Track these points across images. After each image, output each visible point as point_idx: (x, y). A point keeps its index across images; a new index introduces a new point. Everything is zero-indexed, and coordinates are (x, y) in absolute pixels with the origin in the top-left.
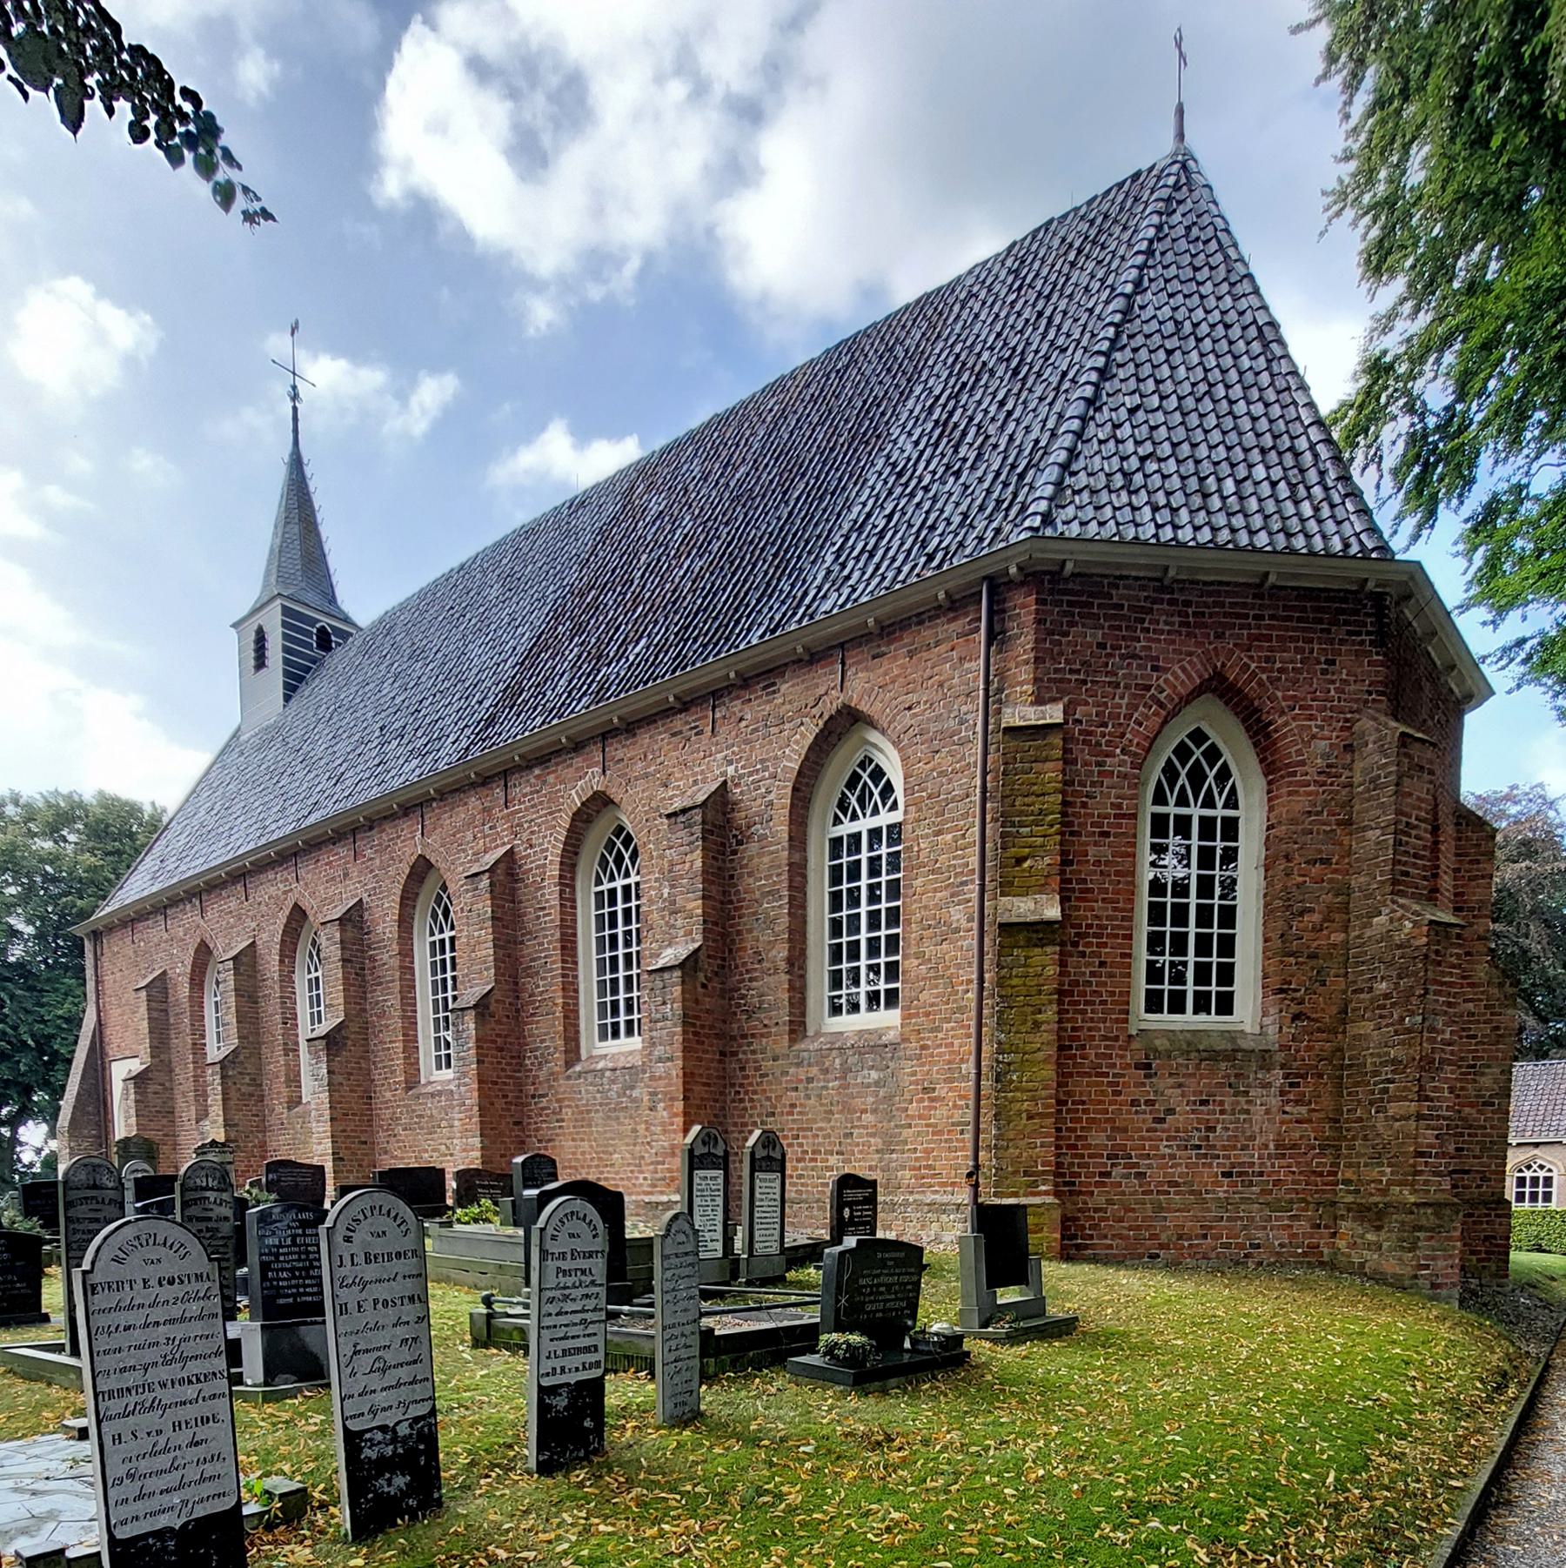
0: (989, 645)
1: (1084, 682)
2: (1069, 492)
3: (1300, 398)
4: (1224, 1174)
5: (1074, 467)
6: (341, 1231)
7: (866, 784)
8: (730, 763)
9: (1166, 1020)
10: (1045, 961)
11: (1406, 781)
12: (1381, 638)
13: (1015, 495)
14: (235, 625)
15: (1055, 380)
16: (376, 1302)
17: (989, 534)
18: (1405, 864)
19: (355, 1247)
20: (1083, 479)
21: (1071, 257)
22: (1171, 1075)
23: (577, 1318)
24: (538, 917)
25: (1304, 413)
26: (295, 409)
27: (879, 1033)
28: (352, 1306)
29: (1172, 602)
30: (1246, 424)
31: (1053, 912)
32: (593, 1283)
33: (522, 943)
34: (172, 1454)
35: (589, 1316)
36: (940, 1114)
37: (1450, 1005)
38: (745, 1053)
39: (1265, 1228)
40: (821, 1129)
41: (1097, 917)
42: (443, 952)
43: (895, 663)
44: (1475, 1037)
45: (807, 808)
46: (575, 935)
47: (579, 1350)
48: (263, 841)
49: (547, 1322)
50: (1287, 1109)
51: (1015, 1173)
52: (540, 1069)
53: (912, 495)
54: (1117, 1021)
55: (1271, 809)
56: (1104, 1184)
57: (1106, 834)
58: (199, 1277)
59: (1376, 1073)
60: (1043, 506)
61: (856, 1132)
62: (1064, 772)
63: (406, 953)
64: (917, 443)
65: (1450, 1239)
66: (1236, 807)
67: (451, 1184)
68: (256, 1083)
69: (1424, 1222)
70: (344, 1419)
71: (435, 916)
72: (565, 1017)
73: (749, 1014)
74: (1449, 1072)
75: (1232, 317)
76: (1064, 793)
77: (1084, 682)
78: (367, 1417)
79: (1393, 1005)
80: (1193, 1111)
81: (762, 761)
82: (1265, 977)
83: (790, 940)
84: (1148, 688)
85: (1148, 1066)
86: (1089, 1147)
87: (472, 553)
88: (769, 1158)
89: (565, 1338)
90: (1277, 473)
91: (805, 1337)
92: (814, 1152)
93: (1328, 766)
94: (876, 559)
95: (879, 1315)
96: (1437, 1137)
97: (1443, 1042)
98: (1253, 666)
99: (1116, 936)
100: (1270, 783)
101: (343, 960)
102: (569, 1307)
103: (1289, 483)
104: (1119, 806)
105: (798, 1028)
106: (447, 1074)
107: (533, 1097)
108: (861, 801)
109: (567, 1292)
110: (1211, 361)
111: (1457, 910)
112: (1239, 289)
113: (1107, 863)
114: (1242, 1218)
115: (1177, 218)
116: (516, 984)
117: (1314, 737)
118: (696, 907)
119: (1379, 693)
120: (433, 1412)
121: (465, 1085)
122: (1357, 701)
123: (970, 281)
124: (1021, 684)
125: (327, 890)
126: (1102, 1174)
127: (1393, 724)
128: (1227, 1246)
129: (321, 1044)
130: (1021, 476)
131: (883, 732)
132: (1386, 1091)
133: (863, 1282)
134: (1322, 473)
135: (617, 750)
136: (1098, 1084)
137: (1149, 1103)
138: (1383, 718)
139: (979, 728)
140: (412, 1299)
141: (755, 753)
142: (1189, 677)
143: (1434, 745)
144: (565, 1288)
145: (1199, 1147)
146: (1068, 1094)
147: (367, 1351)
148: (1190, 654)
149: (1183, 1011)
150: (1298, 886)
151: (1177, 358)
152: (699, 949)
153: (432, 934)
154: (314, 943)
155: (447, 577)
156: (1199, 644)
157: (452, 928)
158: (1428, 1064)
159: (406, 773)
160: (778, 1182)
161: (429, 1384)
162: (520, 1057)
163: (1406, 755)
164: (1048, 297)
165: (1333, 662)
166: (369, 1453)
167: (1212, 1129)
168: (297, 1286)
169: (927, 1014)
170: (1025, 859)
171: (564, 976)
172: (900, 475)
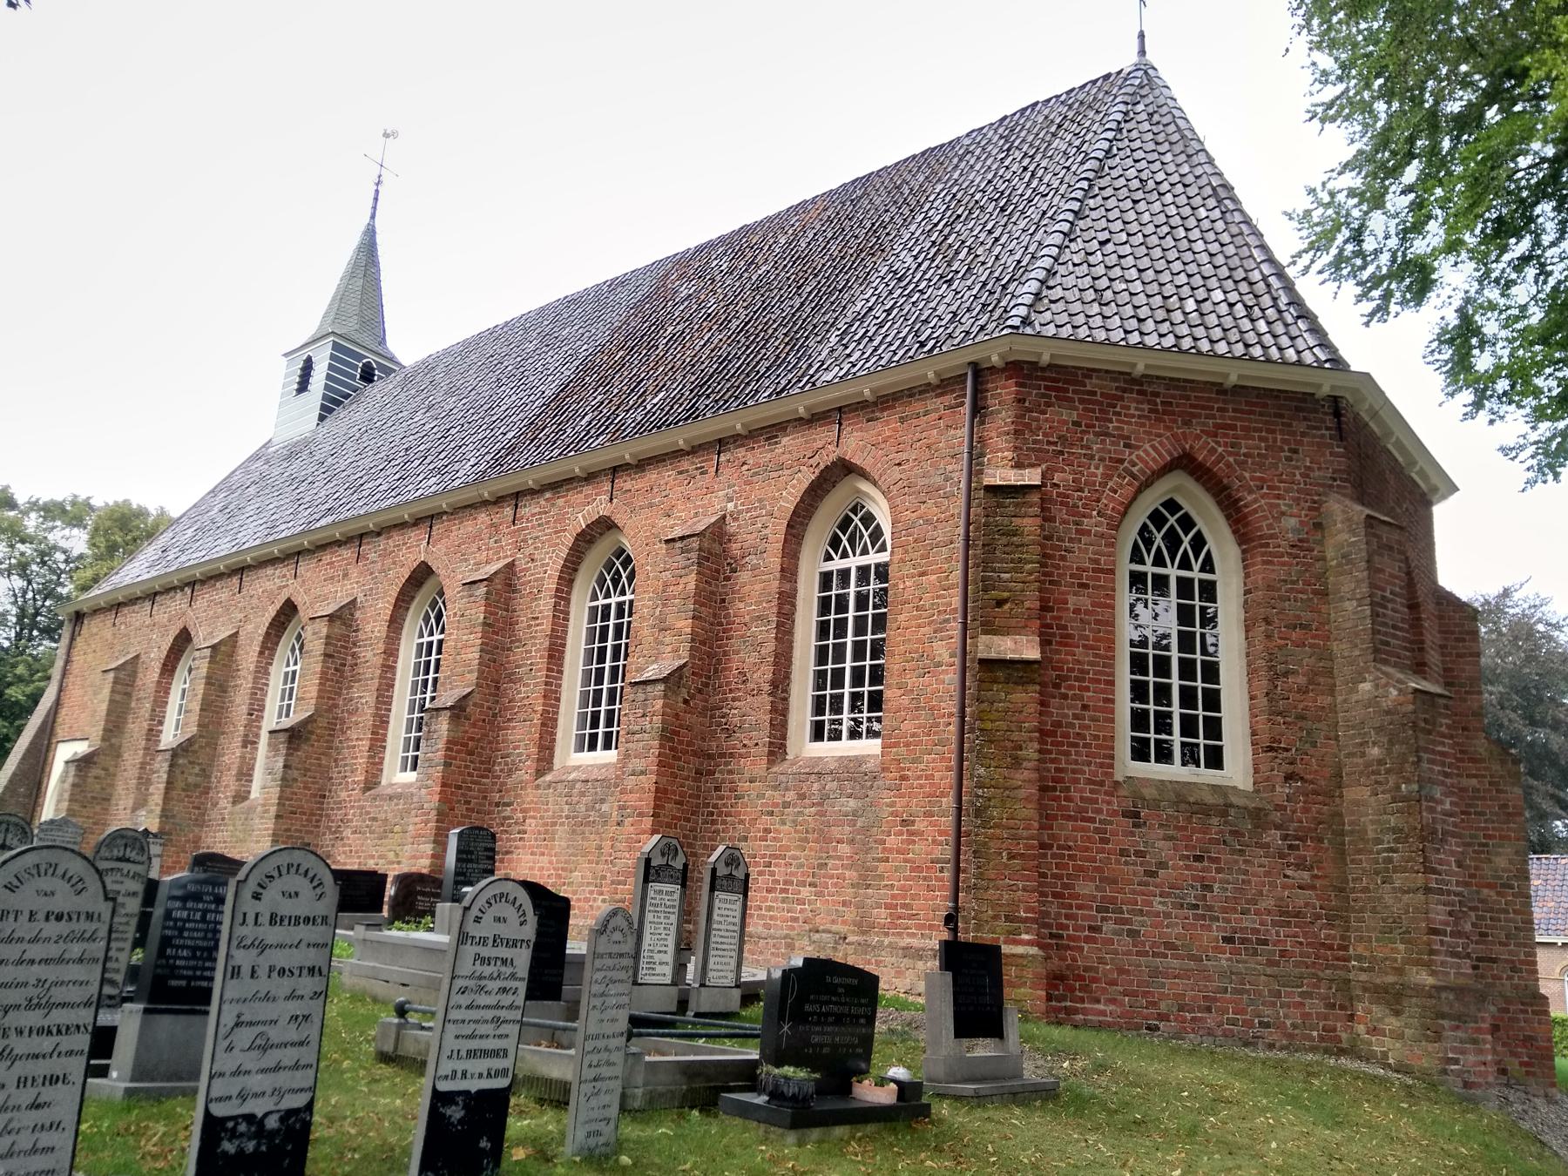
0: (973, 416)
1: (1062, 453)
2: (1046, 301)
3: (1252, 240)
4: (1225, 939)
5: (1051, 283)
6: (252, 886)
7: (853, 528)
8: (730, 500)
9: (1153, 770)
10: (1024, 698)
11: (1376, 558)
12: (1341, 433)
13: (999, 301)
14: (286, 355)
15: (1036, 217)
16: (271, 969)
17: (975, 329)
18: (1386, 634)
19: (264, 908)
20: (1057, 293)
21: (1053, 129)
22: (1161, 826)
23: (489, 1014)
24: (530, 626)
25: (1256, 253)
26: (377, 191)
27: (859, 760)
28: (246, 971)
29: (1140, 392)
30: (1204, 258)
31: (1033, 654)
32: (513, 976)
33: (509, 649)
34: (9, 1115)
35: (503, 1014)
36: (920, 849)
37: (1446, 775)
38: (721, 772)
39: (1274, 1004)
40: (795, 858)
41: (1078, 662)
42: (429, 654)
43: (887, 425)
44: (1483, 814)
45: (800, 544)
46: (564, 645)
47: (486, 1054)
48: (271, 539)
49: (454, 1015)
50: (1289, 873)
51: (996, 917)
52: (509, 776)
53: (909, 296)
54: (1102, 765)
55: (1247, 576)
56: (1094, 940)
57: (1085, 586)
58: (90, 917)
59: (1378, 841)
60: (1023, 311)
61: (831, 862)
62: (1042, 527)
63: (391, 652)
64: (916, 257)
65: (1479, 1030)
66: (1212, 571)
67: (390, 890)
68: (205, 774)
69: (1446, 1009)
70: (208, 1101)
71: (427, 619)
72: (543, 725)
73: (730, 733)
74: (1453, 845)
75: (1189, 179)
76: (1043, 546)
77: (1062, 453)
78: (235, 1101)
79: (1388, 771)
80: (1188, 868)
81: (760, 501)
82: (1254, 734)
83: (775, 664)
84: (1121, 461)
85: (1136, 815)
86: (1077, 896)
87: (518, 314)
88: (730, 876)
89: (472, 1036)
90: (1233, 297)
91: (746, 1075)
92: (786, 882)
93: (1300, 540)
94: (875, 343)
95: (826, 1050)
96: (1450, 914)
97: (1445, 813)
98: (1220, 450)
99: (1098, 681)
100: (1244, 552)
101: (326, 655)
102: (483, 1000)
103: (1245, 306)
104: (1097, 562)
105: (777, 749)
106: (411, 776)
107: (497, 805)
108: (852, 541)
109: (483, 983)
110: (1172, 210)
111: (1447, 685)
112: (1195, 160)
113: (1087, 612)
114: (1248, 991)
115: (1140, 107)
116: (498, 688)
117: (1283, 514)
118: (685, 625)
119: (1345, 480)
120: (309, 1107)
121: (427, 787)
122: (1322, 485)
123: (967, 141)
124: (1001, 450)
125: (319, 589)
126: (1091, 929)
127: (1359, 508)
128: (1234, 1022)
129: (283, 737)
130: (1004, 287)
131: (875, 483)
132: (1389, 860)
133: (808, 1008)
134: (1275, 299)
135: (626, 483)
136: (1083, 829)
137: (1138, 854)
138: (1348, 502)
139: (963, 485)
140: (311, 970)
141: (753, 495)
142: (1160, 454)
143: (1401, 528)
144: (480, 978)
145: (1196, 907)
146: (1052, 837)
147: (251, 1024)
148: (1160, 436)
149: (859, 568)
150: (1280, 648)
151: (1142, 206)
152: (685, 665)
153: (421, 636)
154: (299, 636)
155: (491, 331)
156: (1168, 428)
157: (442, 632)
158: (1429, 836)
159: (425, 487)
160: (739, 904)
161: (311, 1072)
162: (490, 762)
163: (1375, 535)
164: (1032, 157)
165: (1295, 451)
166: (229, 1147)
167: (1209, 888)
168: (195, 968)
169: (907, 745)
170: (1005, 601)
171: (546, 684)
172: (900, 280)
